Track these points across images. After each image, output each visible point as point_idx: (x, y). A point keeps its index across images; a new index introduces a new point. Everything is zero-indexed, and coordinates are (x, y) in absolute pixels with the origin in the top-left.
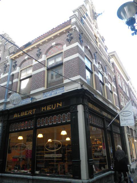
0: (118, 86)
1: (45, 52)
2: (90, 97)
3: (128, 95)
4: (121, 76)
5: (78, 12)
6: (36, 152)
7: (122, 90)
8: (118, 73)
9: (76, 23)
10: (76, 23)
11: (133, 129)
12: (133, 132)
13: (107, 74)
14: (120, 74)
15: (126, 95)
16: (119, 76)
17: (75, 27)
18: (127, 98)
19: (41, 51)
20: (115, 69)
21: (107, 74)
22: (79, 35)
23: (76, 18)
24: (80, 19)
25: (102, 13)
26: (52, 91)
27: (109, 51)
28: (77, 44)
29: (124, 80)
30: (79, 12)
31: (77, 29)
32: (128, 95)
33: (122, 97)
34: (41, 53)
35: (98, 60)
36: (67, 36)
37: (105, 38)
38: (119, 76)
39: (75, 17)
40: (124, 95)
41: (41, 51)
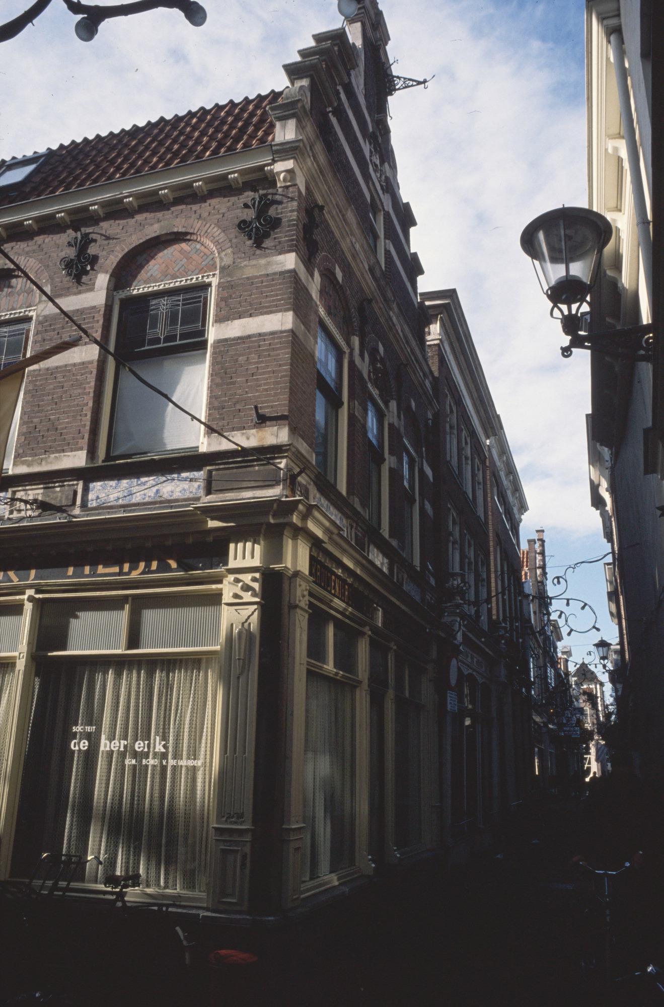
11: (480, 680)
14: (459, 402)
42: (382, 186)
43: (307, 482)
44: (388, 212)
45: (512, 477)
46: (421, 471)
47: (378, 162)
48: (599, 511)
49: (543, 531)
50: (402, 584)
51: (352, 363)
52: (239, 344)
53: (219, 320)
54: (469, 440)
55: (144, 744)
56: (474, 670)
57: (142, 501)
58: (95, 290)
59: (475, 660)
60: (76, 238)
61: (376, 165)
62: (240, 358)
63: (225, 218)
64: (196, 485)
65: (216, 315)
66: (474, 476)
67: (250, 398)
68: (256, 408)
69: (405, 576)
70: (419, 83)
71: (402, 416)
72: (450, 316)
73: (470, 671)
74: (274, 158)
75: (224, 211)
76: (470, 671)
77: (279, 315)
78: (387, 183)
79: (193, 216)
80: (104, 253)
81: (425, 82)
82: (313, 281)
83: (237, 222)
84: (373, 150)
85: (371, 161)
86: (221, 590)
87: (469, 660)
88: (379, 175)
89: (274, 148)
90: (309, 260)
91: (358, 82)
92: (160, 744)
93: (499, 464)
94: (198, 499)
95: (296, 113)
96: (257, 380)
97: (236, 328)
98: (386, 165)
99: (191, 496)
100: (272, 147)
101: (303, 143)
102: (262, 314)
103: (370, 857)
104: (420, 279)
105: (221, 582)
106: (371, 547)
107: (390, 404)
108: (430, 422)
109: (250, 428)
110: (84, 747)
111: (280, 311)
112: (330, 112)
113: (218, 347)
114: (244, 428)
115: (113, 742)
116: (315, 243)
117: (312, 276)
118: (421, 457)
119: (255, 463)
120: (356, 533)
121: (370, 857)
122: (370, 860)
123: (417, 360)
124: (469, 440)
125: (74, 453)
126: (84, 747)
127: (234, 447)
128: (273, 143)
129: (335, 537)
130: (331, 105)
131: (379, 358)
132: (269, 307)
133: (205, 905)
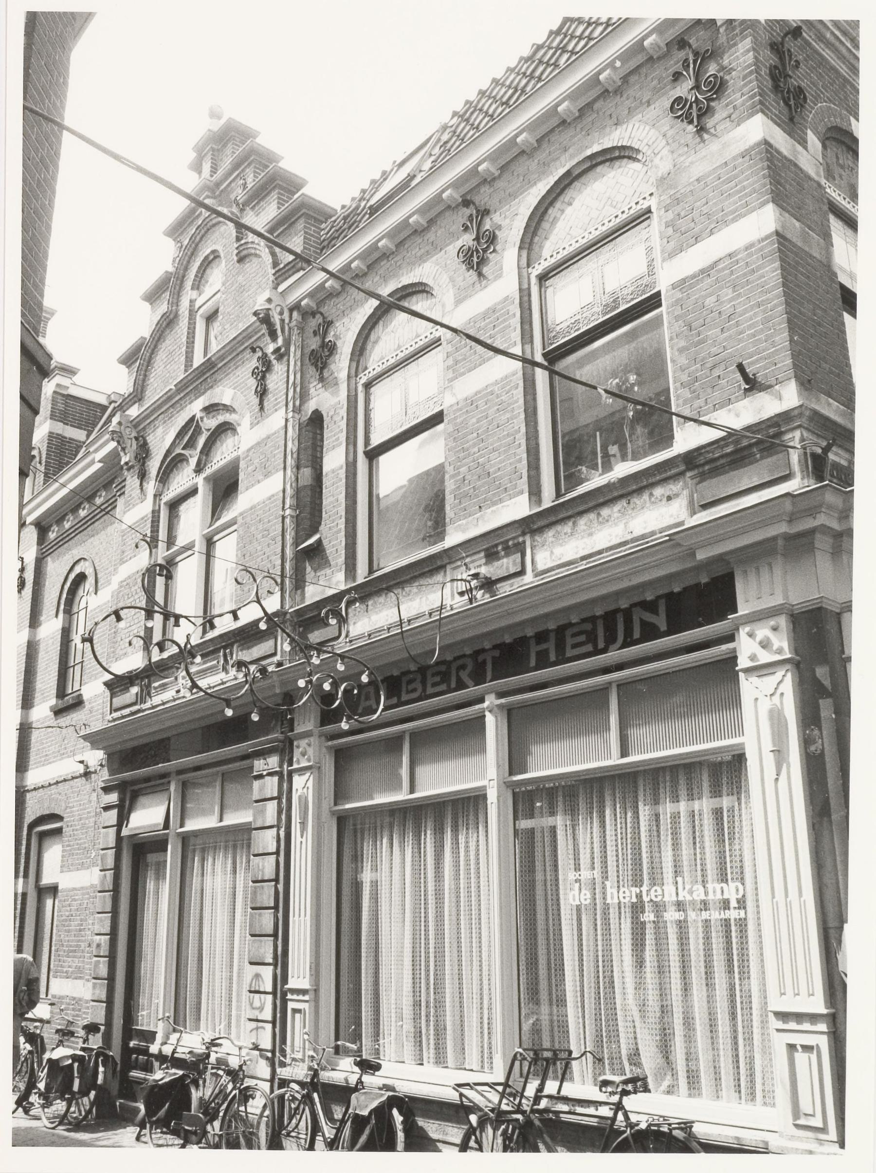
34: (492, 239)
62: (708, 300)
68: (741, 368)
80: (507, 221)
82: (806, 148)
94: (682, 523)
114: (729, 401)
117: (803, 142)
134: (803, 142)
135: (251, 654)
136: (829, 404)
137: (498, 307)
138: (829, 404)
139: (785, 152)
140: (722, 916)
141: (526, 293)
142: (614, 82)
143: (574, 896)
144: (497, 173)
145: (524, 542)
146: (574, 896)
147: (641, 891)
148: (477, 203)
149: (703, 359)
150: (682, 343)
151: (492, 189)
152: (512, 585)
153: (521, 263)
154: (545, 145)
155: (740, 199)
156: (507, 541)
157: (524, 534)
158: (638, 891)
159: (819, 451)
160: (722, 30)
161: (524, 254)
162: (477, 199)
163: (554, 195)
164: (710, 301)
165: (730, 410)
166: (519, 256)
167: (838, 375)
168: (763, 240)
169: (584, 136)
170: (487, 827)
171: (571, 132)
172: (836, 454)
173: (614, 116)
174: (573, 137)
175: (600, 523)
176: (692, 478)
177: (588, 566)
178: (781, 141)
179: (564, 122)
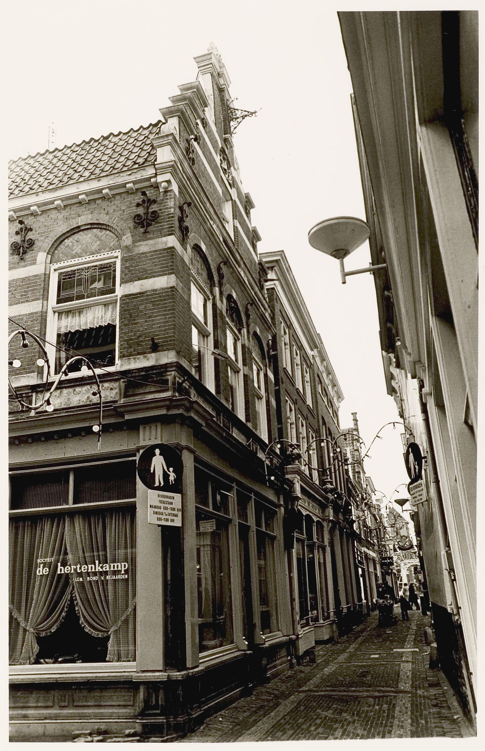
0: (282, 374)
1: (48, 243)
2: (181, 411)
3: (309, 402)
4: (294, 337)
5: (179, 117)
6: (211, 509)
7: (291, 387)
8: (283, 324)
9: (172, 166)
10: (173, 169)
11: (315, 519)
12: (314, 529)
13: (225, 294)
14: (290, 326)
15: (304, 402)
16: (285, 333)
17: (169, 182)
18: (306, 412)
19: (30, 235)
20: (277, 311)
21: (225, 294)
22: (178, 210)
23: (173, 148)
24: (183, 145)
25: (255, 112)
26: (71, 390)
27: (262, 247)
28: (172, 241)
29: (301, 347)
30: (184, 120)
31: (175, 187)
32: (309, 402)
33: (291, 410)
34: (31, 243)
35: (227, 289)
36: (138, 205)
37: (261, 232)
38: (285, 333)
39: (169, 144)
40: (295, 403)
41: (30, 235)
42: (229, 183)
43: (189, 386)
44: (235, 201)
45: (331, 377)
46: (266, 375)
47: (226, 168)
48: (393, 397)
49: (356, 413)
50: (256, 453)
51: (214, 305)
52: (138, 297)
53: (124, 281)
54: (298, 352)
55: (88, 567)
56: (311, 512)
57: (78, 405)
58: (37, 263)
59: (311, 505)
60: (22, 228)
61: (225, 170)
62: (141, 306)
63: (125, 213)
64: (114, 392)
65: (122, 278)
66: (303, 377)
67: (149, 333)
68: (153, 340)
69: (259, 448)
70: (252, 113)
71: (251, 338)
72: (281, 269)
73: (308, 513)
74: (156, 173)
75: (124, 209)
76: (308, 513)
77: (166, 277)
78: (233, 181)
79: (103, 212)
80: (42, 238)
81: (255, 112)
82: (186, 252)
83: (133, 215)
84: (222, 159)
85: (221, 167)
86: (10, 720)
87: (307, 504)
88: (227, 176)
89: (156, 166)
90: (184, 239)
91: (210, 114)
92: (99, 566)
93: (322, 368)
94: (116, 402)
95: (170, 142)
96: (153, 320)
97: (135, 287)
98: (232, 168)
99: (112, 399)
100: (155, 166)
101: (175, 138)
102: (154, 277)
103: (244, 638)
104: (259, 244)
105: (135, 456)
106: (234, 429)
107: (242, 331)
108: (270, 341)
109: (149, 353)
110: (46, 572)
111: (166, 274)
112: (192, 138)
113: (124, 300)
114: (145, 353)
115: (66, 568)
116: (187, 228)
117: (186, 249)
118: (266, 366)
119: (467, 149)
120: (223, 420)
121: (244, 638)
122: (244, 639)
123: (259, 300)
124: (298, 352)
125: (28, 375)
126: (46, 572)
127: (106, 372)
128: (156, 163)
129: (209, 422)
130: (193, 133)
131: (232, 300)
132: (158, 272)
133: (135, 670)
134: (186, 249)
135: (342, 586)
136: (185, 362)
137: (31, 278)
138: (185, 362)
139: (180, 253)
140: (114, 578)
141: (47, 276)
142: (109, 195)
143: (39, 570)
144: (40, 213)
145: (32, 396)
146: (39, 570)
147: (77, 568)
148: (26, 223)
149: (135, 331)
150: (126, 322)
151: (35, 220)
152: (22, 416)
153: (47, 261)
154: (68, 209)
155: (161, 268)
156: (23, 394)
157: (32, 392)
158: (75, 567)
159: (180, 381)
160: (161, 194)
161: (49, 256)
162: (26, 222)
163: (69, 234)
164: (141, 307)
165: (145, 356)
166: (47, 257)
167: (188, 350)
168: (168, 288)
169: (90, 213)
170: (476, 628)
171: (83, 208)
172: (186, 384)
173: (106, 210)
174: (83, 212)
175: (75, 394)
176: (123, 382)
177: (66, 414)
178: (179, 248)
179: (80, 203)
